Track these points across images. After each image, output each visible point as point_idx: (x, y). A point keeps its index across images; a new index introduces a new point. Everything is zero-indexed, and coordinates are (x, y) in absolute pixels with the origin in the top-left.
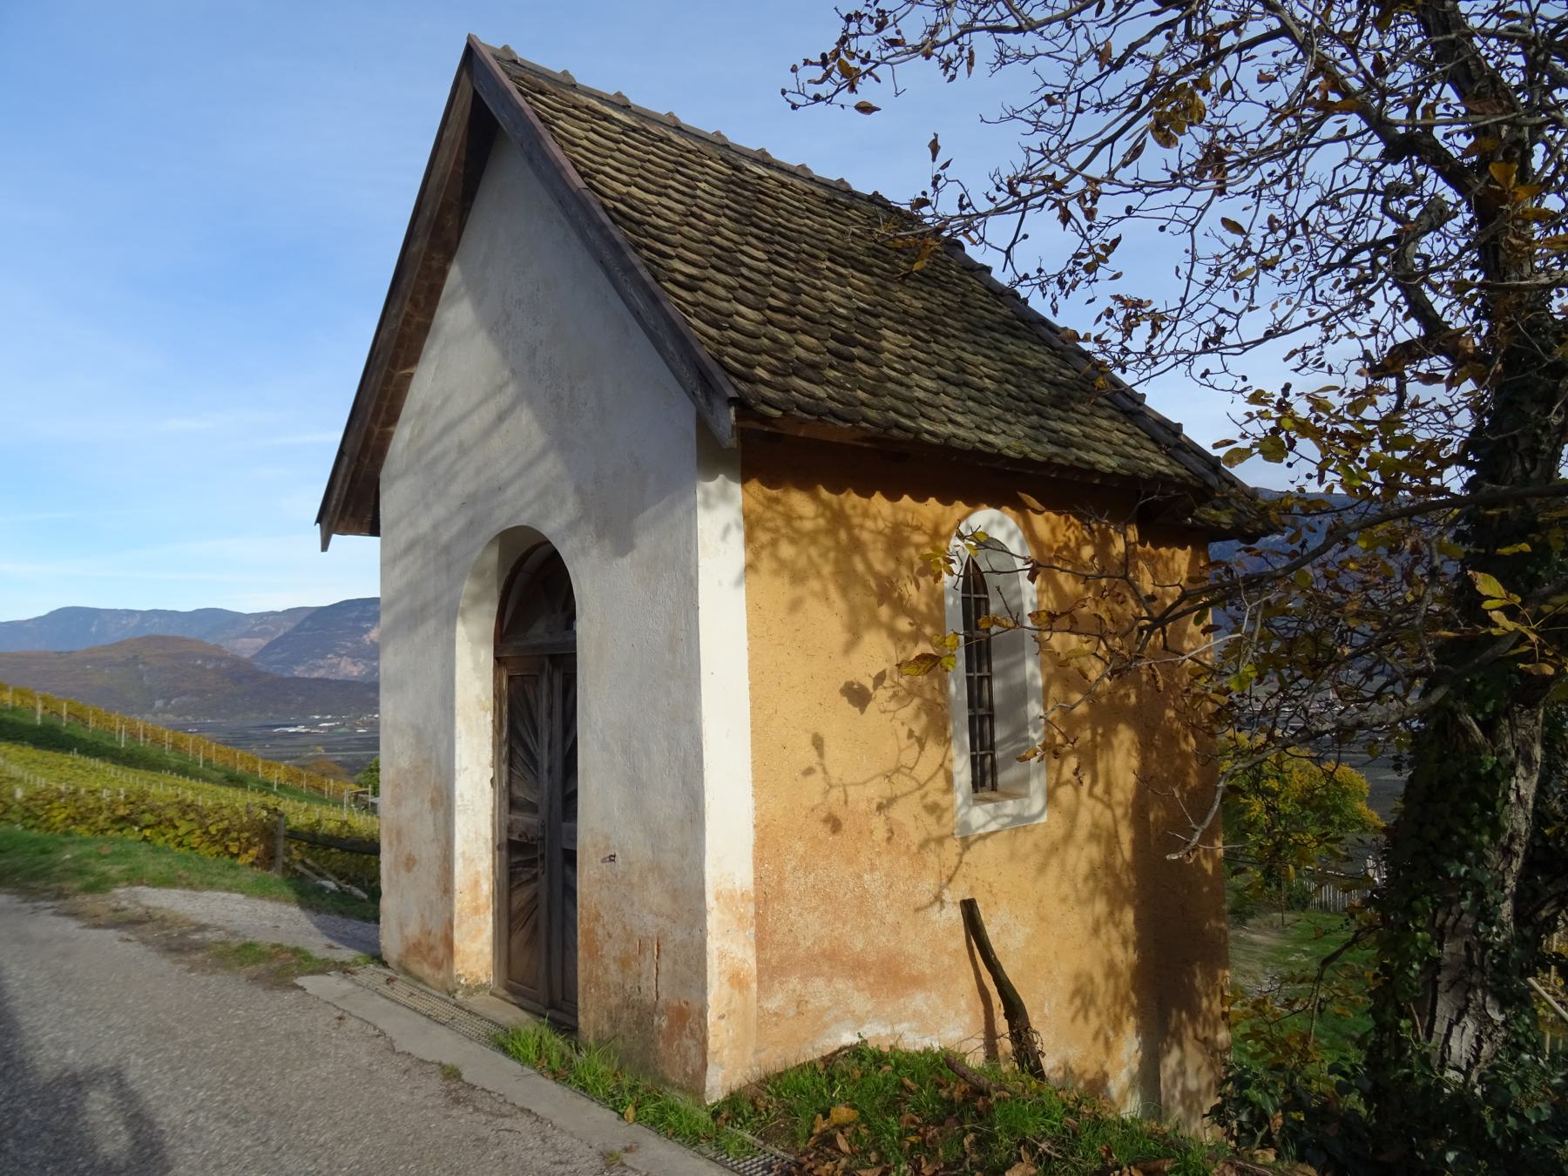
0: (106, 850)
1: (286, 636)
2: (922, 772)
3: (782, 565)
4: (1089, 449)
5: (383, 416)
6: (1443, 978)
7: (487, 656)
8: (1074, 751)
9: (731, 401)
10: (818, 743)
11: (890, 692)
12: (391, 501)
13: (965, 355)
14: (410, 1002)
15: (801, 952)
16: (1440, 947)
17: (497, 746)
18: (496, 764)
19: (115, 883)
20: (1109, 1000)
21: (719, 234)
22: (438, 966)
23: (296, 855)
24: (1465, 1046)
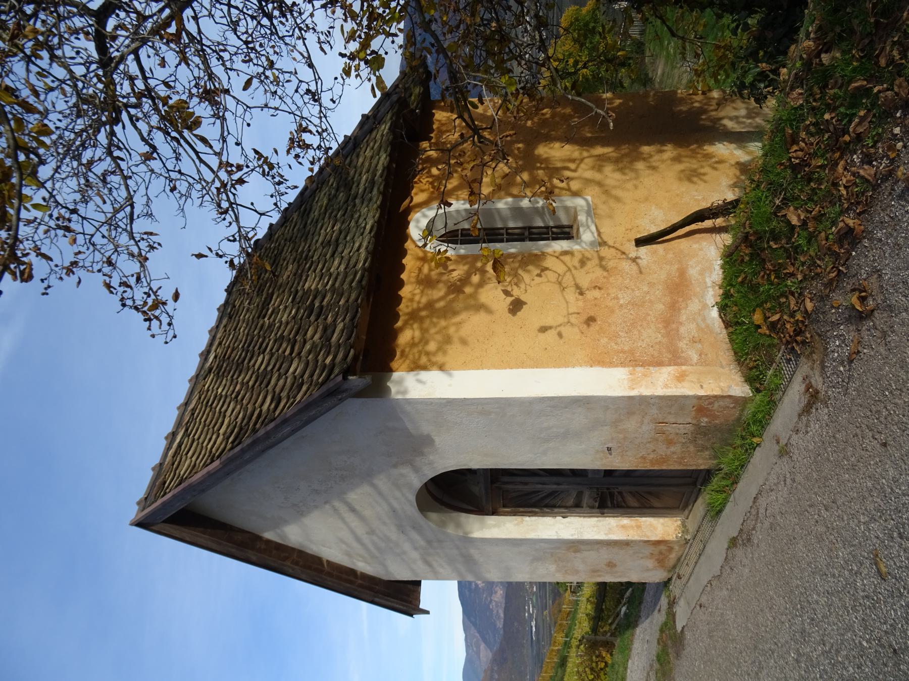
1: (479, 632)
2: (561, 269)
3: (440, 349)
4: (376, 170)
5: (352, 578)
7: (491, 520)
9: (345, 378)
10: (544, 329)
11: (515, 287)
12: (403, 575)
13: (320, 240)
15: (665, 340)
17: (544, 514)
18: (554, 515)
20: (694, 161)
22: (671, 549)
23: (607, 628)
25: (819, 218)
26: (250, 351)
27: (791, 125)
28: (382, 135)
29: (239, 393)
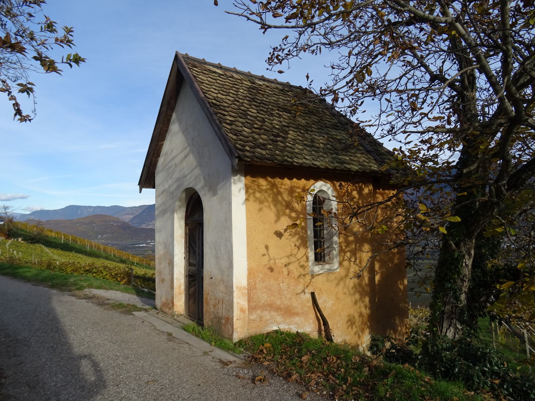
0: (83, 279)
1: (139, 214)
2: (299, 256)
3: (257, 199)
4: (350, 164)
5: (155, 155)
6: (445, 316)
7: (183, 223)
8: (349, 251)
9: (237, 157)
10: (267, 247)
11: (289, 234)
12: (159, 179)
13: (316, 137)
14: (163, 318)
15: (261, 304)
16: (445, 307)
17: (185, 248)
18: (185, 253)
19: (85, 288)
20: (360, 324)
21: (243, 106)
22: (170, 309)
23: (139, 283)
24: (451, 335)
25: (301, 367)
26: (260, 105)
27: (345, 357)
28: (371, 166)
29: (238, 101)
